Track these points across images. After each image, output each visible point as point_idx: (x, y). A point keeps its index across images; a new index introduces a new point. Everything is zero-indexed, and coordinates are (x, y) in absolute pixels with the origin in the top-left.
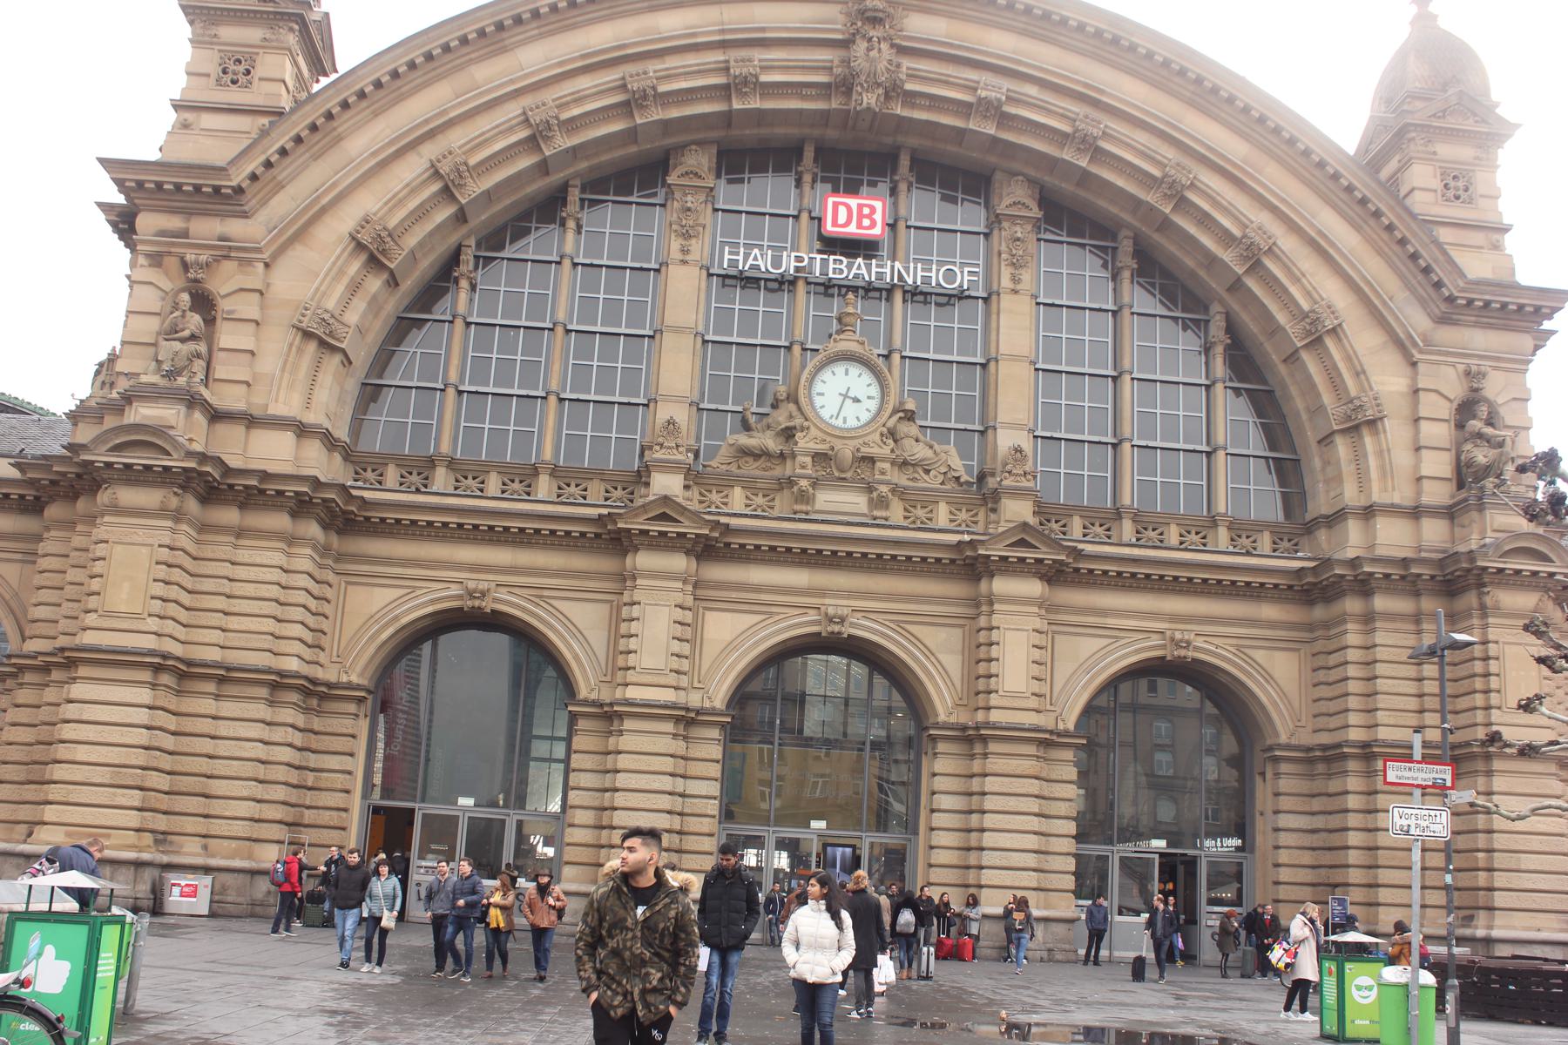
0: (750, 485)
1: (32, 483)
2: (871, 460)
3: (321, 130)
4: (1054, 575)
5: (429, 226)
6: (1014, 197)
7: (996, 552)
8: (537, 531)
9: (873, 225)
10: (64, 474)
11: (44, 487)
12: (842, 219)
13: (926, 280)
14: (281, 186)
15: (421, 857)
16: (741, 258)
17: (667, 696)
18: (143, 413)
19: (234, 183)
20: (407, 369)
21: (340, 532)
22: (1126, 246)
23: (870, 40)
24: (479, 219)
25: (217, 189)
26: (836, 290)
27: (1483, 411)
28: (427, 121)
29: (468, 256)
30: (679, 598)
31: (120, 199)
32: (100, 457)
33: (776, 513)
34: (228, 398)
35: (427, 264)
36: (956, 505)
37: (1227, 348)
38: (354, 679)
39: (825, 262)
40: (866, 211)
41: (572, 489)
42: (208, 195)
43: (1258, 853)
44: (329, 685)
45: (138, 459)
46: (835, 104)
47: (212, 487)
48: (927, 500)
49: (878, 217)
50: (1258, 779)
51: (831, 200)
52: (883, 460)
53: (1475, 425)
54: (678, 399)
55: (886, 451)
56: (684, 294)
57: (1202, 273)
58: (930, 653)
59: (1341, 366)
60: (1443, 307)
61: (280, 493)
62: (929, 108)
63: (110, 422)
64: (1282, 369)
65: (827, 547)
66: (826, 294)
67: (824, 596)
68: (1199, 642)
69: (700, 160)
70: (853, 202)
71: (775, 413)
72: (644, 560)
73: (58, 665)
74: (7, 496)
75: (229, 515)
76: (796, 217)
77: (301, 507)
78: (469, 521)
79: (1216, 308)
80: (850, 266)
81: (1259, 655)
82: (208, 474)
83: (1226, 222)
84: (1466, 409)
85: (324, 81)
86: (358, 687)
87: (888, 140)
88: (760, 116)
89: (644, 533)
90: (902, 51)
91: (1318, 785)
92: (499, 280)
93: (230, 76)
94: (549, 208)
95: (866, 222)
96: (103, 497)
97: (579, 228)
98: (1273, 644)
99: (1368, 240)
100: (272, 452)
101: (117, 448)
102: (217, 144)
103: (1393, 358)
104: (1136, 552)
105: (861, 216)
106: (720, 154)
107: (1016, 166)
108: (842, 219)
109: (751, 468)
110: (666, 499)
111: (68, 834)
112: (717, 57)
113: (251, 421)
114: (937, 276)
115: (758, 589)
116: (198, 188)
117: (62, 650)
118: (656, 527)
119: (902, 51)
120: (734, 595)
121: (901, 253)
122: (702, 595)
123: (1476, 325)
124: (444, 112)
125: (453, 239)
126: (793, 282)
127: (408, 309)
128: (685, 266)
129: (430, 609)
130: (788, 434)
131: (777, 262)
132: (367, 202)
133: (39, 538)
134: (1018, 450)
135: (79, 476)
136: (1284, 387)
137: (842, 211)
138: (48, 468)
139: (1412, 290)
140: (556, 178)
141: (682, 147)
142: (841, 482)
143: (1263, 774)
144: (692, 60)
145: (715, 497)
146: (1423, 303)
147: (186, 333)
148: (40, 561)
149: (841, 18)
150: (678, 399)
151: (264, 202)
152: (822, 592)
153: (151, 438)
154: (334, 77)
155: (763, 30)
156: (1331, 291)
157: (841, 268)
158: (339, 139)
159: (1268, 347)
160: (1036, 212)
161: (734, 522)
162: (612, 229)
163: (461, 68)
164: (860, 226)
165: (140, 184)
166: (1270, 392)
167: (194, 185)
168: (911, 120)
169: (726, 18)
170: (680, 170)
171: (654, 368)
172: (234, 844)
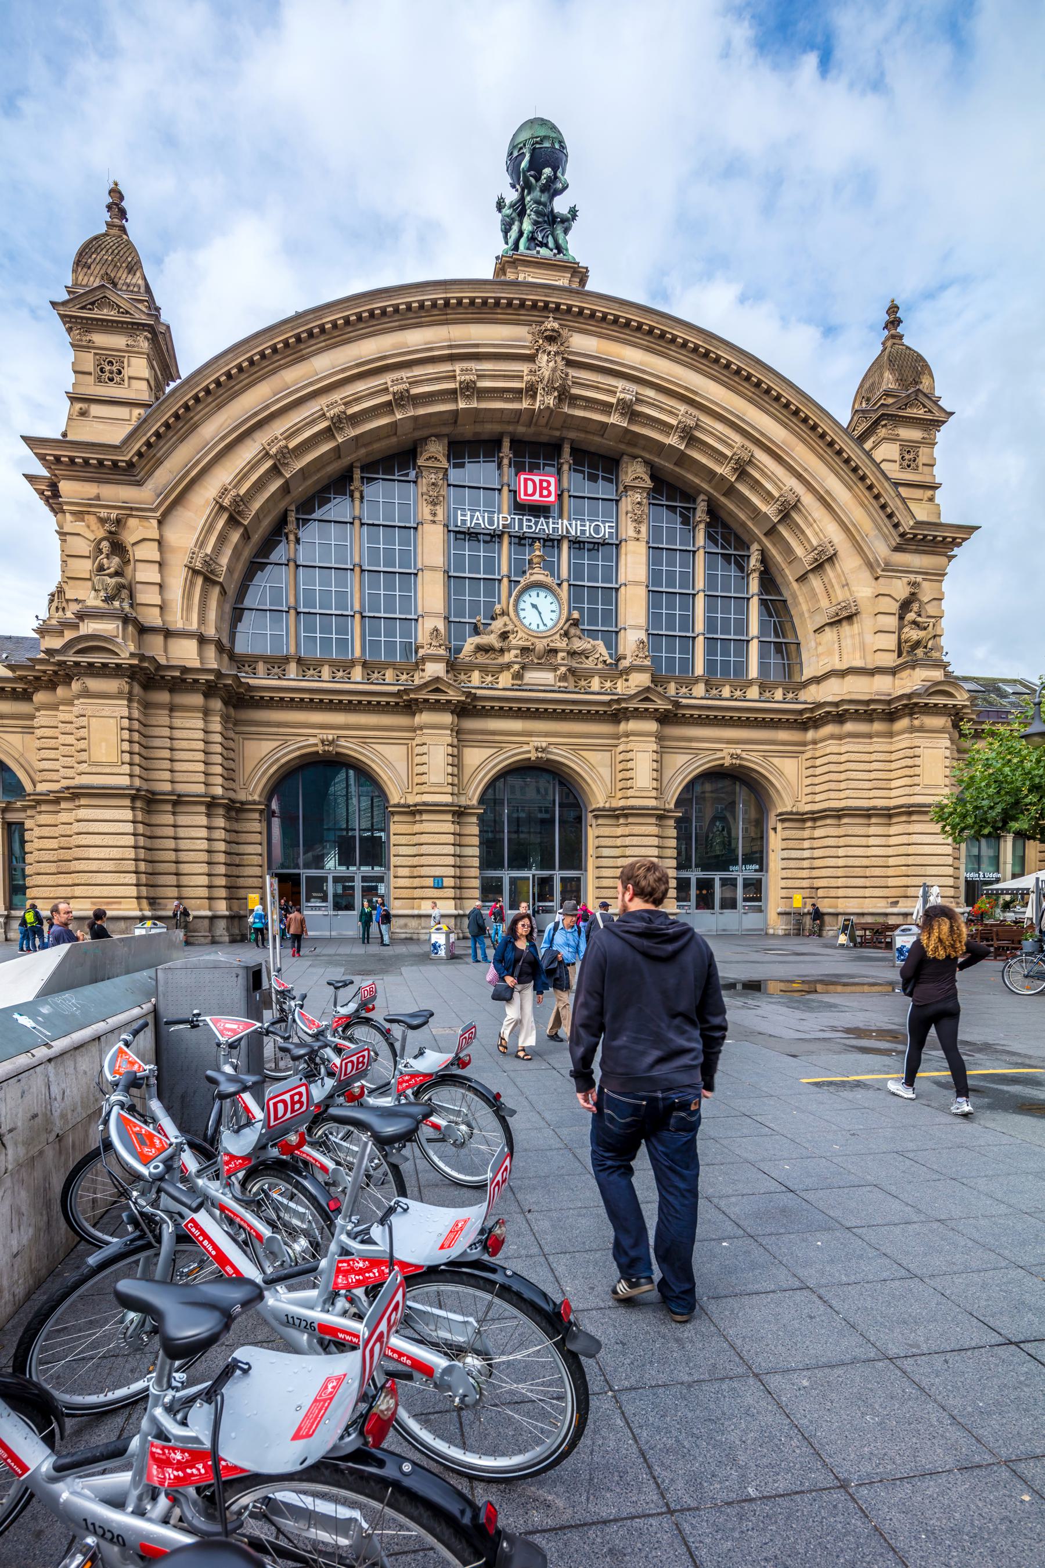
0: (484, 670)
1: (21, 679)
2: (554, 651)
3: (182, 422)
4: (665, 718)
5: (266, 495)
6: (634, 472)
7: (632, 705)
8: (360, 702)
9: (549, 495)
10: (44, 672)
11: (30, 682)
12: (530, 491)
13: (583, 532)
14: (159, 463)
15: (308, 901)
16: (468, 518)
17: (448, 799)
18: (89, 627)
19: (127, 458)
20: (259, 594)
21: (235, 707)
22: (701, 507)
23: (549, 354)
24: (299, 490)
25: (115, 463)
26: (526, 542)
27: (915, 606)
28: (256, 414)
29: (292, 517)
30: (449, 740)
31: (44, 472)
32: (71, 658)
33: (500, 686)
34: (152, 618)
35: (266, 523)
36: (604, 677)
37: (761, 573)
38: (256, 798)
39: (521, 521)
40: (545, 484)
41: (376, 675)
42: (124, 469)
43: (770, 873)
44: (242, 803)
45: (97, 659)
46: (525, 404)
47: (149, 680)
48: (588, 675)
49: (552, 488)
50: (771, 833)
51: (522, 477)
52: (562, 651)
53: (911, 616)
54: (435, 615)
55: (564, 645)
56: (432, 546)
57: (749, 523)
58: (593, 767)
59: (834, 581)
60: (898, 540)
61: (196, 681)
62: (585, 408)
63: (69, 635)
64: (795, 585)
65: (533, 706)
66: (520, 544)
67: (531, 736)
68: (744, 755)
69: (436, 449)
70: (537, 479)
71: (494, 623)
72: (424, 718)
73: (65, 799)
74: (3, 689)
75: (164, 697)
76: (500, 490)
77: (210, 690)
78: (317, 697)
79: (755, 547)
80: (536, 523)
81: (776, 761)
82: (147, 668)
83: (769, 487)
84: (905, 606)
85: (173, 385)
86: (259, 803)
87: (557, 433)
88: (476, 414)
89: (426, 701)
90: (570, 363)
91: (806, 834)
92: (311, 534)
93: (115, 375)
94: (340, 484)
95: (545, 493)
96: (76, 686)
97: (362, 498)
98: (783, 755)
99: (856, 496)
100: (185, 653)
101: (78, 652)
102: (110, 428)
103: (866, 575)
104: (704, 702)
105: (542, 488)
106: (450, 443)
107: (637, 451)
108: (530, 491)
109: (482, 659)
110: (438, 679)
111: (93, 904)
112: (445, 368)
113: (168, 634)
114: (589, 529)
115: (494, 733)
116: (101, 462)
117: (68, 788)
118: (433, 697)
119: (570, 363)
120: (480, 737)
121: (566, 514)
122: (461, 739)
123: (916, 551)
124: (267, 407)
125: (282, 505)
126: (500, 536)
127: (256, 556)
128: (429, 522)
129: (298, 753)
130: (504, 636)
131: (491, 522)
132: (223, 476)
133: (32, 717)
134: (436, 630)
135: (55, 672)
136: (795, 597)
137: (530, 483)
138: (32, 668)
139: (880, 529)
140: (346, 461)
141: (425, 440)
142: (539, 667)
143: (775, 829)
144: (430, 370)
145: (463, 677)
146: (885, 537)
147: (112, 570)
148: (37, 731)
149: (530, 337)
150: (435, 615)
151: (150, 474)
152: (530, 734)
153: (95, 644)
154: (178, 381)
155: (477, 346)
156: (832, 532)
157: (529, 525)
158: (195, 427)
159: (787, 571)
160: (649, 484)
161: (479, 692)
162: (381, 497)
163: (274, 371)
164: (541, 495)
165: (58, 459)
166: (785, 601)
167: (112, 461)
168: (573, 416)
169: (452, 336)
170: (426, 455)
171: (419, 595)
172: (198, 901)
